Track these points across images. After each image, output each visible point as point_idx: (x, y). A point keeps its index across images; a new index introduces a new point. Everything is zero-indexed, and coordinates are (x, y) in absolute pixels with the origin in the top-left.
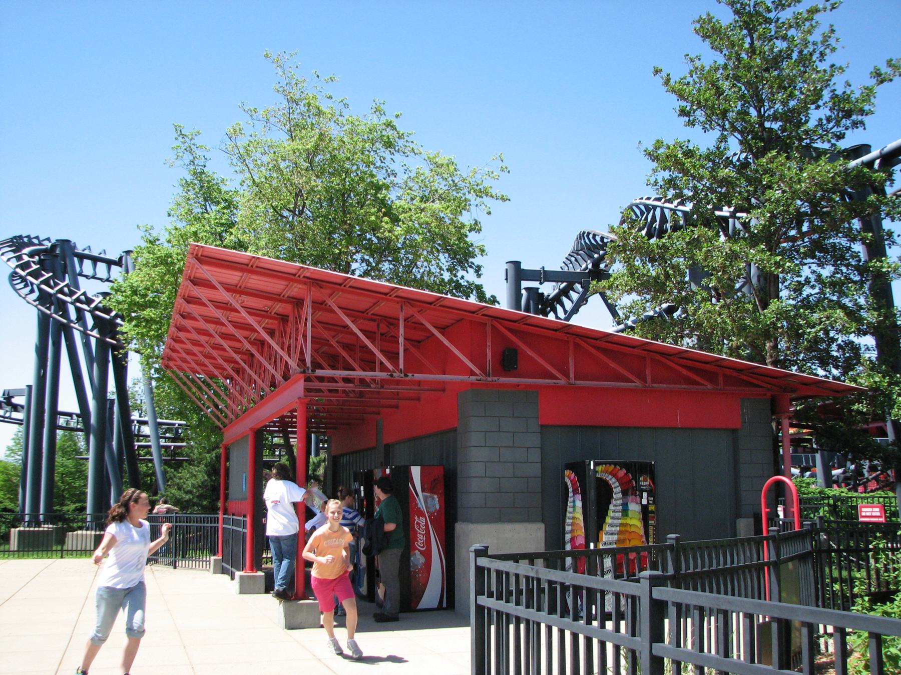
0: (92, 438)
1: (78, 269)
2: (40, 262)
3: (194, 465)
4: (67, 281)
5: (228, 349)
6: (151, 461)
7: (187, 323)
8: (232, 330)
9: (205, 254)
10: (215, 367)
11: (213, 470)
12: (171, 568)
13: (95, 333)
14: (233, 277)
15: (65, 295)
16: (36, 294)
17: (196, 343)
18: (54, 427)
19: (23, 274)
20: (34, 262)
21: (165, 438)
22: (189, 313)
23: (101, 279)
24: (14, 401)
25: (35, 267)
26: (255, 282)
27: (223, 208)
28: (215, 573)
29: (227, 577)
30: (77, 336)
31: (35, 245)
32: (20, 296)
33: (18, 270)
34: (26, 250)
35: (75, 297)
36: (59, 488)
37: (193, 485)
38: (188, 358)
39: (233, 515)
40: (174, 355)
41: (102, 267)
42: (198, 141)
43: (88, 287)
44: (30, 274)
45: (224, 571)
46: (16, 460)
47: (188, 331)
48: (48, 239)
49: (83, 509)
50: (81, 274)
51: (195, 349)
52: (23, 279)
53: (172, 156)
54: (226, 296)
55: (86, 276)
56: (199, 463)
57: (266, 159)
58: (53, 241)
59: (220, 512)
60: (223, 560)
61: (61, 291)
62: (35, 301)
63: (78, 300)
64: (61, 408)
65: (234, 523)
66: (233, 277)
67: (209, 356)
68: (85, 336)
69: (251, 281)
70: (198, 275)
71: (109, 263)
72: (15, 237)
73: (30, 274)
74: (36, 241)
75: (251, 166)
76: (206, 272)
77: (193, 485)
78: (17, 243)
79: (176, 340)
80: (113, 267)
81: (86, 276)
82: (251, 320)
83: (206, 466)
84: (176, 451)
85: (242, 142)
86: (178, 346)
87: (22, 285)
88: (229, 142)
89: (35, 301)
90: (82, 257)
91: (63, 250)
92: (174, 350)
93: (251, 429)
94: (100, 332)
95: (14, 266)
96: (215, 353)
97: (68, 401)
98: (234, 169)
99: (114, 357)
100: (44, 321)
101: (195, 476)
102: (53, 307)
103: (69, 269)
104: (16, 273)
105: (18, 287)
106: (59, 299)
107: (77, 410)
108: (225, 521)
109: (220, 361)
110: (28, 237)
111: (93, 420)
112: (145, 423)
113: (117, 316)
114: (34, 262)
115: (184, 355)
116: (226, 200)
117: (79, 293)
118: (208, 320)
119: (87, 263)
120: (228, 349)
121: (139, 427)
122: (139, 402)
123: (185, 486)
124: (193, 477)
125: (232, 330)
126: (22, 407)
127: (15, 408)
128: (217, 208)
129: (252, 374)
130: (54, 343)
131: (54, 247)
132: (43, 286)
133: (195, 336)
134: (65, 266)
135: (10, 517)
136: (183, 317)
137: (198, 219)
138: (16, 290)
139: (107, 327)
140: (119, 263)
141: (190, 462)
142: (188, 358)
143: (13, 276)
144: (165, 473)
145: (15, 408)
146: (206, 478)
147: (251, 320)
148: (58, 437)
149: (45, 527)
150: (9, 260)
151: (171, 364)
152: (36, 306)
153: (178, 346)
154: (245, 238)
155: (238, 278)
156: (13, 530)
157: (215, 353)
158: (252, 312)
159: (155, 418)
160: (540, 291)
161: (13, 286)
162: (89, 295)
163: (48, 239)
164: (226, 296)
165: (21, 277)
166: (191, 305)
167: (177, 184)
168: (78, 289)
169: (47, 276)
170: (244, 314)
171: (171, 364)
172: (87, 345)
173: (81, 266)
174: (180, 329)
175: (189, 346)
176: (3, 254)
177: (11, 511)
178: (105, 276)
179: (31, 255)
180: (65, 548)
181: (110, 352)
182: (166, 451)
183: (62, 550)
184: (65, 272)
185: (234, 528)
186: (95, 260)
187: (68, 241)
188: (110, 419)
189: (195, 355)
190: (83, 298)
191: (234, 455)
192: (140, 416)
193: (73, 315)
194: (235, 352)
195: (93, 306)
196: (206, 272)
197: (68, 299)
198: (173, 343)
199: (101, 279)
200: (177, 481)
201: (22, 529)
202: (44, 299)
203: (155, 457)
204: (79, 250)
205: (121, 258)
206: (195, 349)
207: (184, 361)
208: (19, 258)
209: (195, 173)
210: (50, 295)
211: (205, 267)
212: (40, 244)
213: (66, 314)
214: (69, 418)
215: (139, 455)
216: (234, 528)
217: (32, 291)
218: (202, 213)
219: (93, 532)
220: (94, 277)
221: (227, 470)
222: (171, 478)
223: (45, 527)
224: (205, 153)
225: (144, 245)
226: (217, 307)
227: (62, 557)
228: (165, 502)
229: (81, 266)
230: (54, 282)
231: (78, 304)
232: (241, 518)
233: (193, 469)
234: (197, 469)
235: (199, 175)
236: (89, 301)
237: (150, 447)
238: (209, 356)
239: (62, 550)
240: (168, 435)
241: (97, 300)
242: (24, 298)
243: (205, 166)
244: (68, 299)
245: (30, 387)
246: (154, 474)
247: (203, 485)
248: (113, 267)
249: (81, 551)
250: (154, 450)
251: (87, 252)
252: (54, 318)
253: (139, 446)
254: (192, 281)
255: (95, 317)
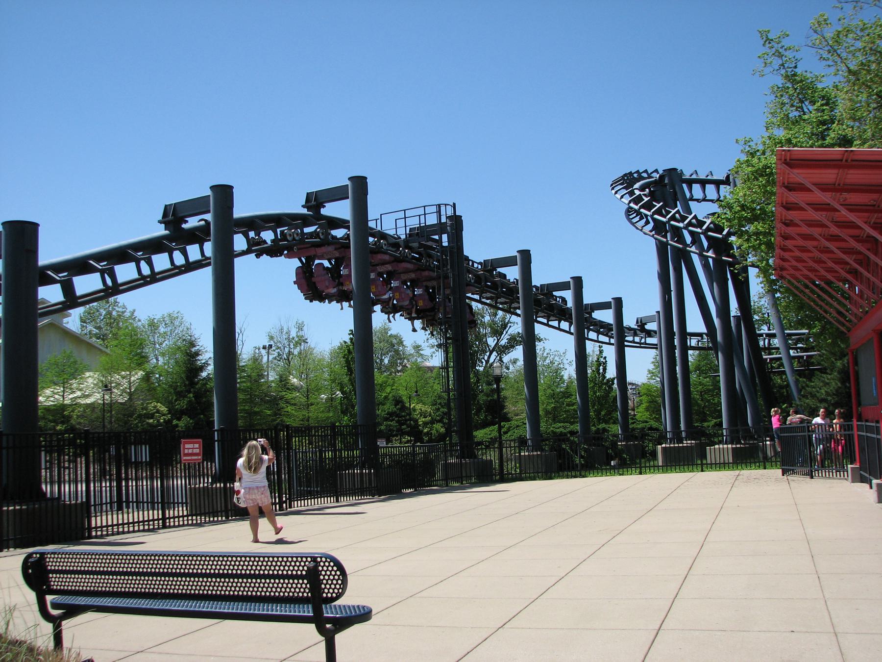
0: (720, 354)
1: (688, 195)
2: (651, 194)
3: (827, 373)
4: (679, 207)
5: (835, 250)
6: (784, 372)
7: (791, 231)
8: (834, 230)
9: (794, 157)
10: (827, 271)
11: (845, 375)
12: (808, 479)
13: (710, 254)
14: (829, 176)
15: (678, 221)
16: (652, 224)
17: (803, 250)
18: (685, 348)
19: (636, 207)
20: (645, 195)
21: (796, 349)
22: (791, 221)
23: (712, 201)
24: (648, 327)
25: (646, 199)
26: (854, 176)
27: (822, 105)
28: (853, 482)
29: (866, 486)
30: (696, 259)
31: (645, 178)
32: (637, 228)
33: (632, 205)
34: (637, 186)
35: (686, 222)
36: (699, 405)
37: (827, 394)
38: (799, 265)
39: (867, 421)
40: (786, 264)
41: (710, 189)
42: (785, 42)
43: (700, 210)
44: (642, 207)
45: (863, 480)
46: (655, 382)
47: (793, 239)
48: (656, 171)
49: (721, 424)
50: (692, 199)
51: (804, 256)
52: (638, 213)
53: (760, 65)
54: (825, 197)
55: (697, 200)
56: (832, 370)
57: (860, 44)
58: (661, 172)
59: (854, 420)
60: (860, 469)
61: (673, 218)
62: (651, 231)
63: (690, 224)
64: (689, 329)
65: (869, 429)
66: (829, 176)
67: (820, 262)
68: (704, 259)
69: (849, 176)
70: (791, 180)
71: (717, 183)
72: (625, 175)
73: (642, 207)
74: (645, 175)
75: (844, 55)
76: (798, 176)
77: (827, 394)
78: (628, 181)
79: (784, 249)
80: (722, 187)
81: (697, 200)
82: (852, 217)
83: (839, 373)
84: (808, 361)
85: (829, 34)
86: (786, 255)
87: (637, 219)
88: (815, 36)
89: (651, 231)
90: (690, 182)
91: (670, 179)
92: (783, 260)
93: (874, 331)
94: (715, 252)
95: (627, 202)
96: (824, 257)
97: (695, 323)
98: (825, 63)
99: (732, 272)
100: (662, 249)
101: (828, 384)
102: (669, 235)
103: (679, 195)
104: (631, 208)
105: (634, 220)
106: (672, 226)
107: (703, 330)
108: (860, 428)
109: (830, 264)
110: (638, 172)
111: (719, 338)
112: (773, 336)
113: (729, 234)
114: (645, 195)
115: (794, 263)
116: (823, 98)
117: (690, 217)
118: (811, 224)
119: (696, 188)
120: (835, 250)
121: (769, 341)
122: (766, 316)
123: (818, 395)
124: (827, 384)
125: (834, 230)
126: (655, 332)
127: (649, 333)
128: (815, 107)
129: (869, 276)
130: (675, 269)
131: (662, 177)
132: (656, 216)
133: (800, 242)
134: (675, 194)
135: (656, 435)
136: (786, 225)
137: (796, 122)
138: (633, 224)
139: (721, 246)
140: (727, 182)
141: (823, 371)
142: (799, 265)
143: (629, 211)
144: (797, 382)
145: (649, 333)
146: (839, 384)
147: (852, 217)
148: (690, 359)
149: (686, 443)
150: (622, 197)
151: (784, 273)
152: (653, 236)
153: (786, 255)
154: (849, 132)
155: (835, 176)
156: (659, 447)
157: (824, 257)
158: (852, 208)
159: (782, 328)
160: (392, 332)
161: (630, 220)
162: (700, 218)
163: (656, 171)
164: (825, 197)
165: (636, 211)
166: (790, 212)
167: (768, 93)
168: (690, 213)
169: (658, 205)
170: (844, 212)
171: (784, 273)
172: (706, 266)
173: (691, 192)
174: (786, 237)
175: (797, 253)
176: (616, 193)
177: (657, 429)
178: (715, 197)
179: (642, 189)
180: (704, 462)
181: (727, 270)
182: (799, 362)
183: (702, 464)
184: (675, 200)
185: (869, 435)
186: (703, 183)
187: (675, 169)
188: (735, 336)
189: (804, 261)
190: (694, 221)
191: (862, 359)
192: (769, 330)
193: (688, 239)
194: (844, 253)
195: (704, 228)
196: (798, 176)
197: (681, 225)
198: (782, 253)
199: (712, 201)
200: (809, 389)
201: (664, 445)
202: (659, 228)
203: (787, 368)
204: (687, 175)
205: (728, 177)
206: (804, 256)
207: (796, 269)
208: (631, 193)
209: (787, 77)
210: (664, 224)
211: (796, 171)
212: (649, 177)
213: (681, 239)
214: (699, 338)
215: (772, 367)
216: (869, 435)
217: (647, 223)
218: (800, 116)
219: (730, 446)
220: (704, 200)
221: (857, 374)
222: (803, 387)
223: (686, 443)
224: (795, 53)
225: (744, 158)
226: (817, 210)
227: (702, 471)
228: (796, 413)
229: (691, 192)
230: (666, 211)
231: (690, 228)
232: (874, 424)
233: (826, 377)
234: (829, 377)
235: (792, 78)
236: (700, 224)
237: (780, 359)
238: (820, 262)
239: (702, 464)
240: (800, 345)
241: (708, 222)
242: (641, 230)
243: (796, 67)
244: (681, 225)
245: (658, 312)
246: (788, 385)
247: (837, 393)
248: (722, 187)
249: (720, 464)
250: (785, 361)
251: (694, 177)
252: (670, 245)
253: (771, 359)
254: (786, 187)
255: (708, 238)
